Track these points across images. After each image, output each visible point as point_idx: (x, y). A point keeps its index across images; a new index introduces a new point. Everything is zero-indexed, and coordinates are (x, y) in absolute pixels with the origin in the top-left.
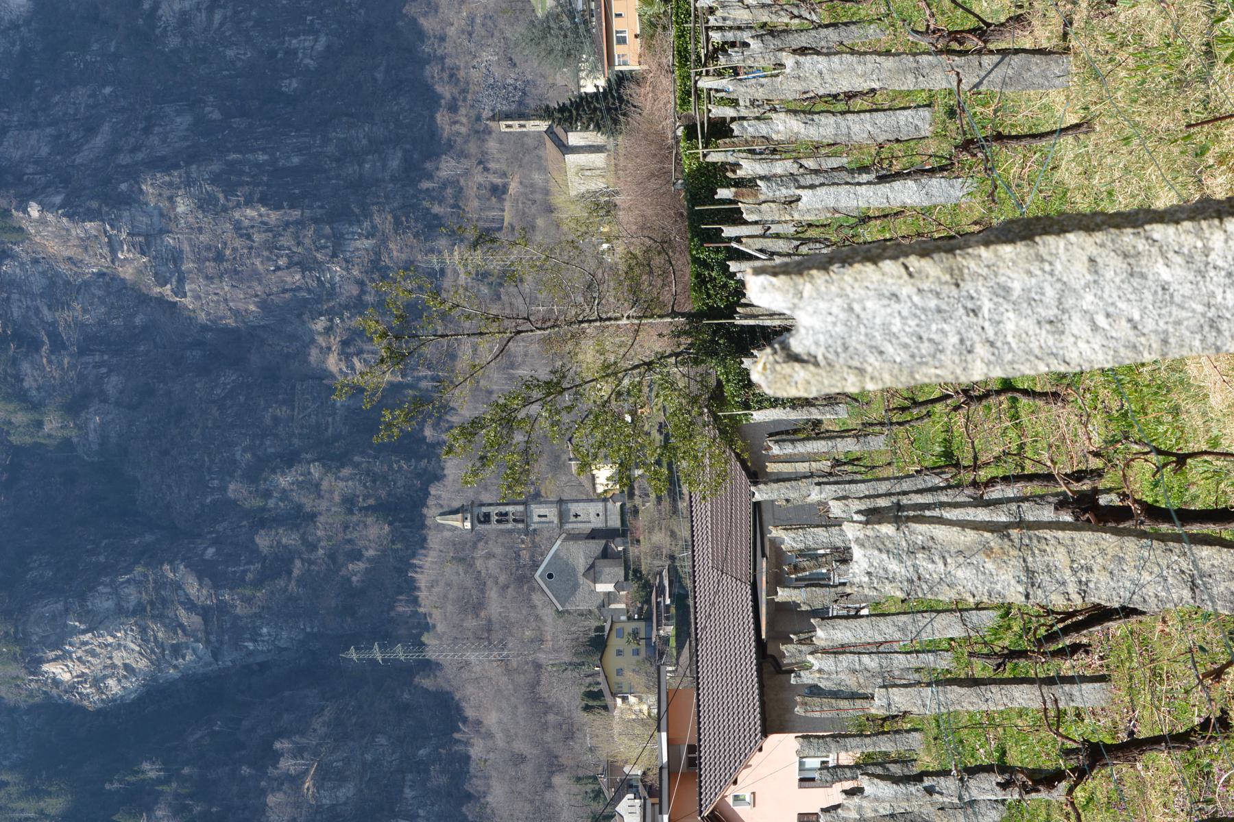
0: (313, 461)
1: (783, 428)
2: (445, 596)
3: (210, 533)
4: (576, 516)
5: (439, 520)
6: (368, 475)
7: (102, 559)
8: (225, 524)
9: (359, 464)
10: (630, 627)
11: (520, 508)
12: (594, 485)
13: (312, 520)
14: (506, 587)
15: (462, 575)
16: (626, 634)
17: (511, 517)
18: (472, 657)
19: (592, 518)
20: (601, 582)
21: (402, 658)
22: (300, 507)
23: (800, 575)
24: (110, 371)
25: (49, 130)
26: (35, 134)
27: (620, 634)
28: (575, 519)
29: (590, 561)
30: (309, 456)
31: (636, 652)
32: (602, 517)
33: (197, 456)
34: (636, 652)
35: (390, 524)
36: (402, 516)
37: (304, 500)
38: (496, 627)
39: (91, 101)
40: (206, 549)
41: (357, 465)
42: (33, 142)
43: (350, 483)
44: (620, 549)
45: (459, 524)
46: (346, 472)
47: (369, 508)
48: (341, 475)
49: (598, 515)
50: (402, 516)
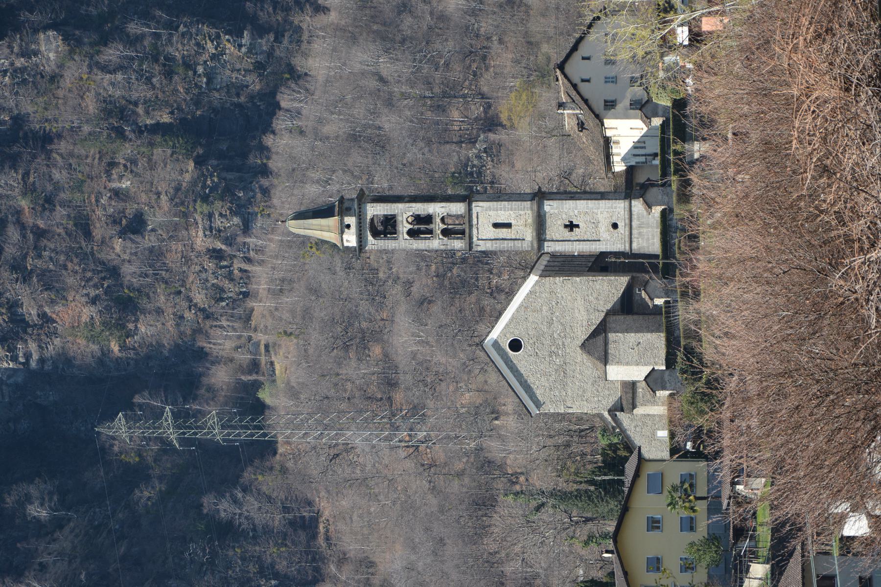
0: (46, 28)
2: (307, 314)
4: (571, 226)
5: (296, 227)
6: (156, 60)
9: (140, 38)
10: (676, 471)
11: (458, 208)
12: (608, 156)
13: (43, 147)
14: (424, 302)
15: (341, 274)
16: (667, 487)
17: (438, 226)
18: (357, 437)
20: (619, 363)
22: (19, 120)
27: (657, 484)
28: (567, 234)
29: (598, 318)
30: (35, 18)
31: (689, 525)
32: (622, 229)
34: (689, 525)
35: (200, 162)
36: (224, 147)
37: (28, 108)
38: (406, 379)
41: (133, 41)
43: (119, 76)
44: (659, 302)
45: (331, 237)
46: (112, 53)
47: (157, 128)
48: (102, 58)
49: (615, 226)
50: (224, 147)
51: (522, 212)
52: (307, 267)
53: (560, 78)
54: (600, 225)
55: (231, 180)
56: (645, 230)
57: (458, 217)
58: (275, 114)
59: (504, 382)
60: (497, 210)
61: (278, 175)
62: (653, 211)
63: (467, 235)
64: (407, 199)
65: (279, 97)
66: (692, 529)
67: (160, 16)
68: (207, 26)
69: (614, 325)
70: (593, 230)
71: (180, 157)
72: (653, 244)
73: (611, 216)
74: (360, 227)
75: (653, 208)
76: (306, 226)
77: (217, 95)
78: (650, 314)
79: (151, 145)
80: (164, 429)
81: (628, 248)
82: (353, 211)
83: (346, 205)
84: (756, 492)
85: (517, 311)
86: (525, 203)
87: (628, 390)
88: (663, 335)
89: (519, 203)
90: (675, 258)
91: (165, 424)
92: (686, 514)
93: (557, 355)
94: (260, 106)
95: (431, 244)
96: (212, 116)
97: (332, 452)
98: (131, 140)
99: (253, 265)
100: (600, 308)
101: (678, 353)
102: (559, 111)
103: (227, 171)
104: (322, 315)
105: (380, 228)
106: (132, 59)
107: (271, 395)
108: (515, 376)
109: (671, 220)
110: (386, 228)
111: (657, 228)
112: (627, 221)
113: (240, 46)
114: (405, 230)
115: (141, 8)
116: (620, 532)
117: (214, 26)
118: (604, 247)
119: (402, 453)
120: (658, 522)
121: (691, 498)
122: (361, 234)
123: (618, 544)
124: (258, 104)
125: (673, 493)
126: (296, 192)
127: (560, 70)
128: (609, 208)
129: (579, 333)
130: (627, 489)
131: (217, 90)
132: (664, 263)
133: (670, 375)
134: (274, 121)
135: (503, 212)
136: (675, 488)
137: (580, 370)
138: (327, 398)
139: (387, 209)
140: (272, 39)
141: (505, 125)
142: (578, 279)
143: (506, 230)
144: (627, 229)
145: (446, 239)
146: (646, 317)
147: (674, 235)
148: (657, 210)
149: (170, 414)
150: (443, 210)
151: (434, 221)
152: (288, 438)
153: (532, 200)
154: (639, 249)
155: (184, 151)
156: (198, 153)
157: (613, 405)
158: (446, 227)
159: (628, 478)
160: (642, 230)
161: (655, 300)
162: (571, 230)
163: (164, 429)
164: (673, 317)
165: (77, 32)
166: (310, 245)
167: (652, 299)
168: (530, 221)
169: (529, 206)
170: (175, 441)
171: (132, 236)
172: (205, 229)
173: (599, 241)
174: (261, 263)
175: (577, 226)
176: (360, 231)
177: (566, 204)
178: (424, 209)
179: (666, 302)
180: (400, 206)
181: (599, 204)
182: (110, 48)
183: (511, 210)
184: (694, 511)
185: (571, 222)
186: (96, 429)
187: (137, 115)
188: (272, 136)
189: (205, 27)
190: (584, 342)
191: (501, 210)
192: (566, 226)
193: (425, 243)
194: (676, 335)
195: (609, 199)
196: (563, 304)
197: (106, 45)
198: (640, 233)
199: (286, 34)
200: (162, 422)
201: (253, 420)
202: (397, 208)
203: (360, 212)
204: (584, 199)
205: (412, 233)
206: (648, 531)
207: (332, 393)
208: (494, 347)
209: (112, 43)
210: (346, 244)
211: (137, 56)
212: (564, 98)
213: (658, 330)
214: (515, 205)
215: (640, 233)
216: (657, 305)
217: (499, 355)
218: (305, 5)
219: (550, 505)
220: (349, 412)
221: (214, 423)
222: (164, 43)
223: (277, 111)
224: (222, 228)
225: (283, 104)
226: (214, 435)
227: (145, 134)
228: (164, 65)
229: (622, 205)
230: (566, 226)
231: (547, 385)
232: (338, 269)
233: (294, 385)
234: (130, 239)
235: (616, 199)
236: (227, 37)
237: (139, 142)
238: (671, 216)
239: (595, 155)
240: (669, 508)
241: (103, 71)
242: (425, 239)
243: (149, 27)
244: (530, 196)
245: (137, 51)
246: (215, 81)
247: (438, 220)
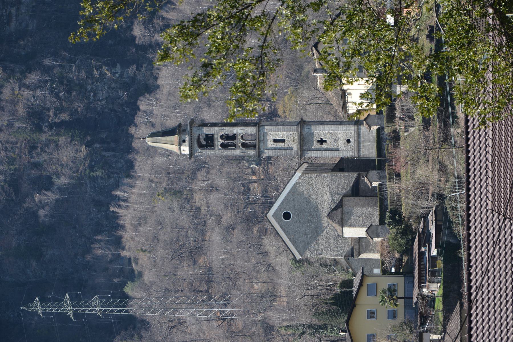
2: (155, 237)
4: (321, 141)
5: (150, 142)
6: (62, 83)
10: (385, 282)
11: (251, 130)
12: (344, 103)
14: (231, 228)
15: (177, 211)
16: (380, 291)
17: (239, 141)
19: (342, 144)
20: (351, 226)
21: (100, 313)
27: (373, 290)
28: (318, 146)
29: (338, 199)
31: (393, 315)
34: (393, 315)
38: (218, 277)
41: (46, 70)
43: (38, 92)
44: (375, 184)
45: (174, 148)
46: (33, 78)
47: (63, 124)
48: (27, 81)
49: (348, 141)
50: (104, 136)
51: (291, 133)
52: (156, 209)
53: (315, 54)
54: (339, 140)
55: (108, 156)
56: (367, 144)
57: (252, 135)
58: (136, 113)
60: (276, 131)
61: (138, 152)
62: (372, 129)
63: (257, 147)
64: (220, 125)
65: (139, 103)
66: (394, 317)
67: (65, 55)
68: (94, 61)
69: (347, 203)
70: (335, 144)
71: (76, 142)
72: (372, 152)
73: (346, 136)
74: (192, 141)
75: (372, 127)
76: (158, 141)
77: (99, 103)
78: (370, 196)
79: (58, 134)
80: (65, 307)
81: (356, 155)
82: (187, 131)
83: (183, 128)
84: (434, 292)
86: (293, 127)
87: (356, 243)
88: (378, 208)
89: (290, 127)
90: (385, 157)
91: (65, 304)
92: (391, 307)
93: (313, 222)
94: (126, 110)
95: (235, 153)
96: (97, 117)
97: (171, 324)
98: (45, 132)
99: (122, 209)
100: (340, 193)
101: (387, 213)
102: (314, 74)
103: (106, 151)
104: (165, 238)
105: (204, 143)
106: (47, 81)
107: (132, 290)
109: (383, 134)
110: (207, 142)
111: (374, 143)
112: (356, 138)
113: (115, 73)
114: (219, 143)
115: (52, 50)
116: (352, 317)
117: (98, 60)
118: (342, 154)
119: (215, 324)
120: (374, 313)
121: (395, 297)
122: (192, 146)
123: (350, 327)
124: (126, 109)
126: (149, 162)
127: (315, 48)
128: (344, 130)
129: (326, 208)
130: (355, 294)
131: (101, 101)
132: (378, 160)
133: (382, 229)
134: (136, 118)
135: (279, 133)
136: (384, 292)
138: (168, 290)
139: (208, 131)
140: (135, 69)
141: (281, 116)
142: (325, 175)
143: (281, 143)
144: (356, 143)
145: (244, 149)
146: (367, 198)
147: (385, 143)
148: (374, 128)
149: (68, 297)
150: (243, 131)
151: (237, 138)
152: (143, 313)
153: (298, 125)
154: (363, 155)
155: (79, 139)
156: (88, 140)
157: (347, 253)
158: (244, 141)
159: (355, 290)
160: (365, 144)
161: (374, 239)
162: (321, 144)
163: (65, 307)
164: (384, 191)
165: (12, 65)
166: (158, 194)
167: (371, 183)
168: (296, 138)
169: (295, 129)
170: (71, 316)
171: (46, 193)
172: (91, 188)
173: (339, 150)
174: (127, 207)
175: (325, 141)
176: (192, 144)
177: (318, 127)
178: (231, 131)
179: (379, 185)
180: (216, 128)
181: (339, 128)
182: (33, 75)
183: (285, 131)
184: (396, 305)
185: (322, 139)
186: (22, 308)
187: (49, 116)
188: (134, 128)
189: (93, 62)
190: (329, 213)
191: (278, 131)
192: (318, 141)
193: (231, 152)
194: (385, 204)
195: (345, 125)
196: (316, 190)
197: (30, 73)
198: (364, 146)
199: (144, 66)
200: (63, 303)
201: (121, 302)
202: (214, 129)
203: (191, 132)
204: (329, 125)
205: (223, 146)
206: (368, 318)
207: (171, 287)
208: (274, 217)
209: (34, 71)
210: (183, 152)
211: (50, 80)
212: (317, 66)
213: (375, 206)
214: (287, 128)
215: (364, 146)
216: (374, 187)
217: (277, 222)
218: (156, 48)
219: (308, 333)
220: (182, 297)
221: (96, 303)
222: (67, 71)
223: (138, 112)
224: (103, 187)
225: (142, 107)
226: (96, 311)
227: (54, 128)
228: (67, 85)
229: (353, 128)
230: (318, 141)
231: (306, 240)
232: (175, 209)
233: (147, 283)
234: (44, 194)
235: (349, 125)
236: (106, 67)
237: (50, 133)
238: (383, 132)
239: (336, 103)
240: (381, 303)
241: (28, 89)
242: (232, 149)
243: (57, 62)
244: (296, 123)
245: (49, 76)
246: (99, 95)
247: (240, 137)
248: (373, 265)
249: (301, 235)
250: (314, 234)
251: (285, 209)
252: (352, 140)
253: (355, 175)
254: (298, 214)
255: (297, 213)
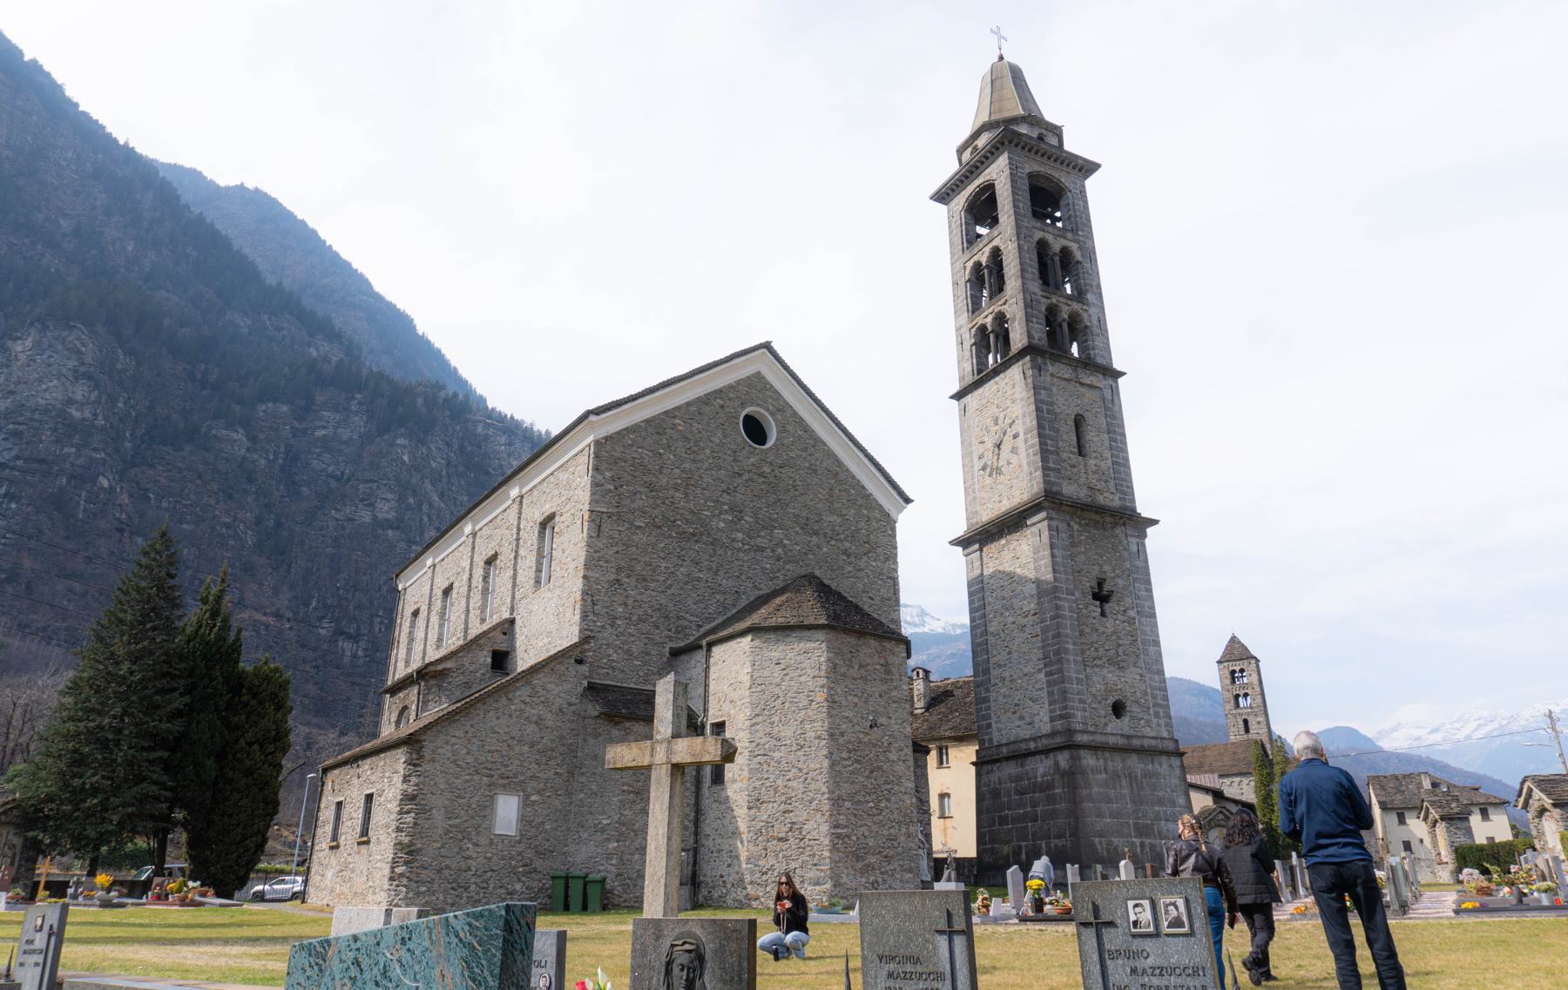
1: (806, 633)
3: (122, 488)
7: (120, 405)
8: (127, 501)
23: (275, 887)
24: (270, 461)
25: (444, 473)
26: (443, 462)
32: (1116, 728)
33: (192, 496)
39: (458, 502)
40: (109, 480)
42: (439, 460)
49: (1118, 709)
59: (525, 457)
73: (1137, 702)
85: (831, 455)
108: (688, 404)
125: (253, 850)
137: (699, 579)
208: (754, 375)
215: (1116, 776)
217: (738, 382)
231: (664, 480)
248: (539, 793)
249: (687, 466)
250: (688, 522)
251: (782, 430)
252: (1123, 725)
253: (1196, 812)
254: (762, 475)
255: (767, 469)
